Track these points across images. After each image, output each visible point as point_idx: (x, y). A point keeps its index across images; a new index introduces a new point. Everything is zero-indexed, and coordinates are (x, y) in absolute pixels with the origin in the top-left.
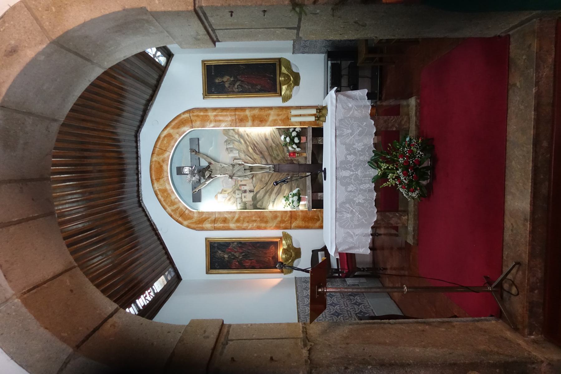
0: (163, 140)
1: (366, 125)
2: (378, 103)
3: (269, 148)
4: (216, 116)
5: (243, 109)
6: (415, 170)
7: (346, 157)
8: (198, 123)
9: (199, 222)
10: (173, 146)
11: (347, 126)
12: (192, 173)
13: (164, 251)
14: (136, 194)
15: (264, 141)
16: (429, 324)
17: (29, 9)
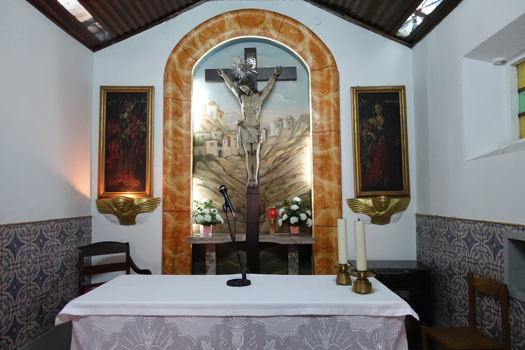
5: (338, 142)
7: (270, 338)
8: (318, 78)
9: (177, 80)
15: (291, 173)
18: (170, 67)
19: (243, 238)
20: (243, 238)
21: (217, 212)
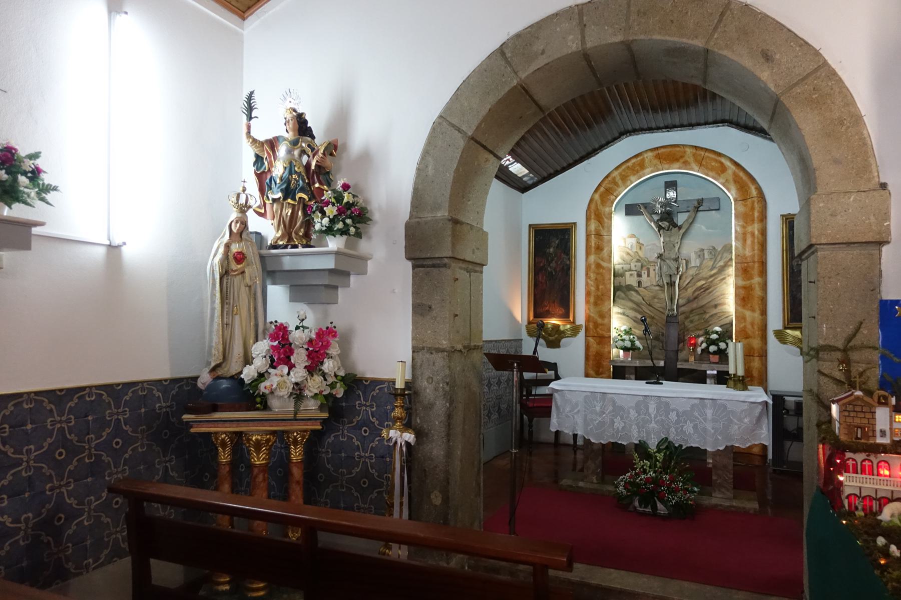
0: (716, 161)
1: (717, 439)
2: (770, 470)
3: (703, 310)
4: (753, 234)
5: (763, 272)
6: (652, 493)
7: (673, 410)
8: (742, 209)
9: (598, 216)
10: (707, 175)
11: (713, 415)
12: (667, 203)
13: (559, 168)
14: (637, 127)
15: (713, 303)
16: (479, 470)
17: (816, 70)
18: (593, 206)
19: (662, 364)
20: (662, 364)
21: (636, 339)
